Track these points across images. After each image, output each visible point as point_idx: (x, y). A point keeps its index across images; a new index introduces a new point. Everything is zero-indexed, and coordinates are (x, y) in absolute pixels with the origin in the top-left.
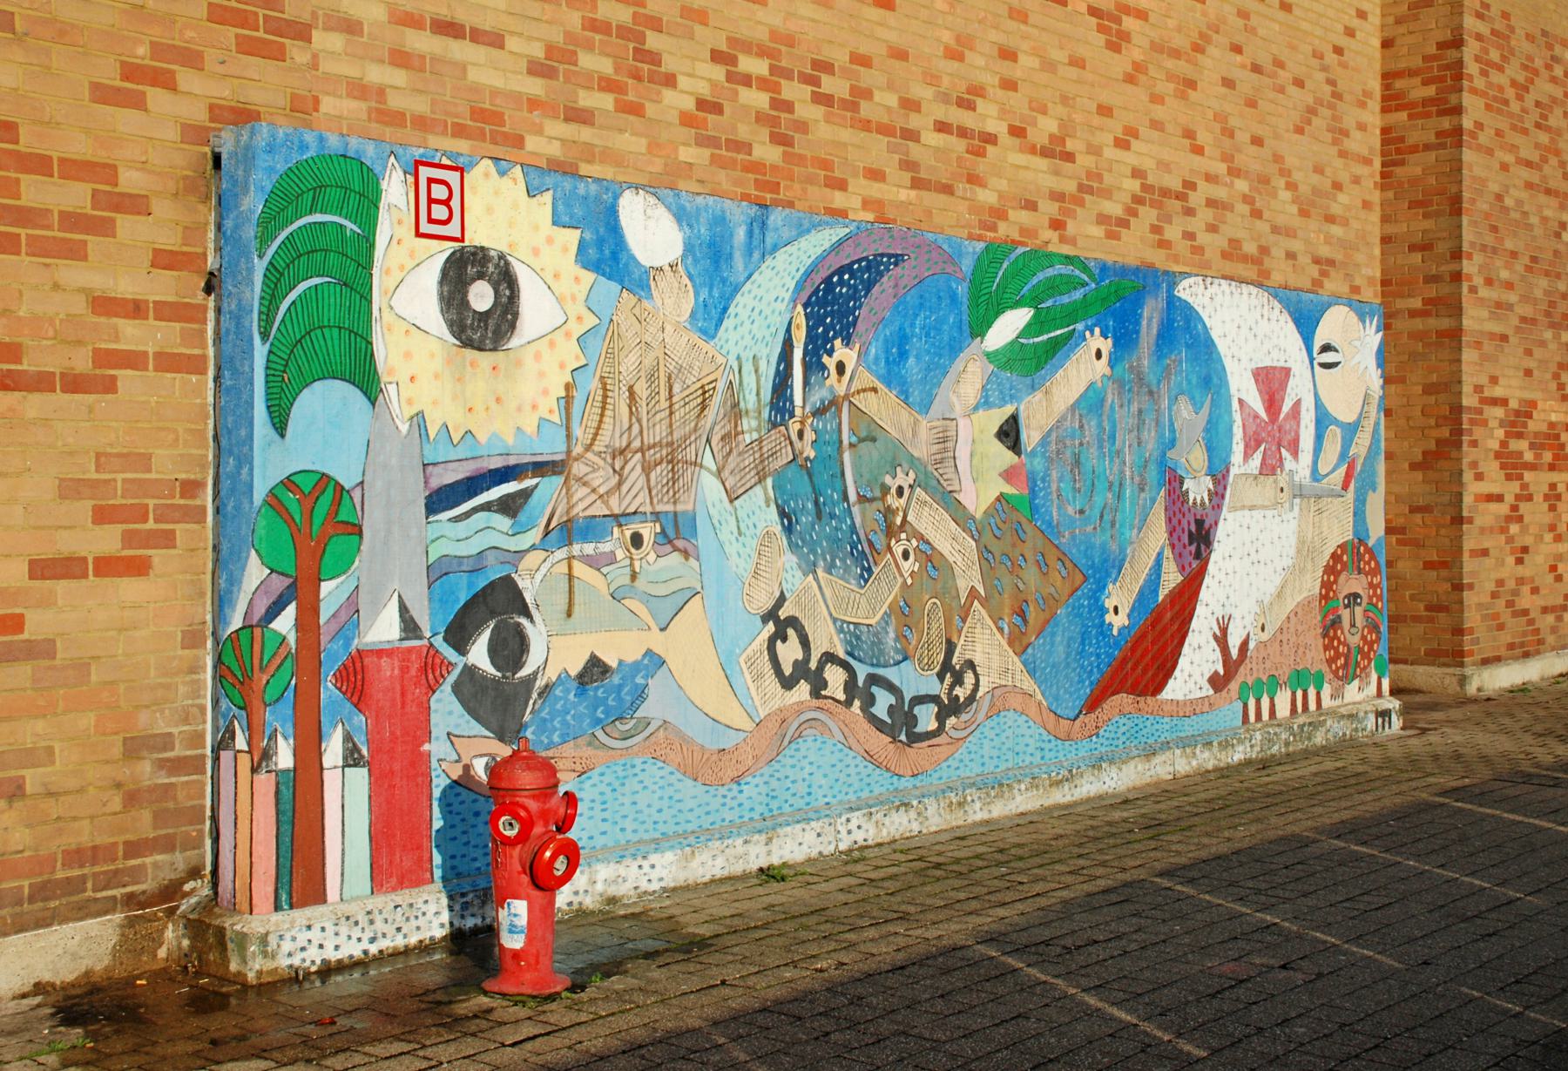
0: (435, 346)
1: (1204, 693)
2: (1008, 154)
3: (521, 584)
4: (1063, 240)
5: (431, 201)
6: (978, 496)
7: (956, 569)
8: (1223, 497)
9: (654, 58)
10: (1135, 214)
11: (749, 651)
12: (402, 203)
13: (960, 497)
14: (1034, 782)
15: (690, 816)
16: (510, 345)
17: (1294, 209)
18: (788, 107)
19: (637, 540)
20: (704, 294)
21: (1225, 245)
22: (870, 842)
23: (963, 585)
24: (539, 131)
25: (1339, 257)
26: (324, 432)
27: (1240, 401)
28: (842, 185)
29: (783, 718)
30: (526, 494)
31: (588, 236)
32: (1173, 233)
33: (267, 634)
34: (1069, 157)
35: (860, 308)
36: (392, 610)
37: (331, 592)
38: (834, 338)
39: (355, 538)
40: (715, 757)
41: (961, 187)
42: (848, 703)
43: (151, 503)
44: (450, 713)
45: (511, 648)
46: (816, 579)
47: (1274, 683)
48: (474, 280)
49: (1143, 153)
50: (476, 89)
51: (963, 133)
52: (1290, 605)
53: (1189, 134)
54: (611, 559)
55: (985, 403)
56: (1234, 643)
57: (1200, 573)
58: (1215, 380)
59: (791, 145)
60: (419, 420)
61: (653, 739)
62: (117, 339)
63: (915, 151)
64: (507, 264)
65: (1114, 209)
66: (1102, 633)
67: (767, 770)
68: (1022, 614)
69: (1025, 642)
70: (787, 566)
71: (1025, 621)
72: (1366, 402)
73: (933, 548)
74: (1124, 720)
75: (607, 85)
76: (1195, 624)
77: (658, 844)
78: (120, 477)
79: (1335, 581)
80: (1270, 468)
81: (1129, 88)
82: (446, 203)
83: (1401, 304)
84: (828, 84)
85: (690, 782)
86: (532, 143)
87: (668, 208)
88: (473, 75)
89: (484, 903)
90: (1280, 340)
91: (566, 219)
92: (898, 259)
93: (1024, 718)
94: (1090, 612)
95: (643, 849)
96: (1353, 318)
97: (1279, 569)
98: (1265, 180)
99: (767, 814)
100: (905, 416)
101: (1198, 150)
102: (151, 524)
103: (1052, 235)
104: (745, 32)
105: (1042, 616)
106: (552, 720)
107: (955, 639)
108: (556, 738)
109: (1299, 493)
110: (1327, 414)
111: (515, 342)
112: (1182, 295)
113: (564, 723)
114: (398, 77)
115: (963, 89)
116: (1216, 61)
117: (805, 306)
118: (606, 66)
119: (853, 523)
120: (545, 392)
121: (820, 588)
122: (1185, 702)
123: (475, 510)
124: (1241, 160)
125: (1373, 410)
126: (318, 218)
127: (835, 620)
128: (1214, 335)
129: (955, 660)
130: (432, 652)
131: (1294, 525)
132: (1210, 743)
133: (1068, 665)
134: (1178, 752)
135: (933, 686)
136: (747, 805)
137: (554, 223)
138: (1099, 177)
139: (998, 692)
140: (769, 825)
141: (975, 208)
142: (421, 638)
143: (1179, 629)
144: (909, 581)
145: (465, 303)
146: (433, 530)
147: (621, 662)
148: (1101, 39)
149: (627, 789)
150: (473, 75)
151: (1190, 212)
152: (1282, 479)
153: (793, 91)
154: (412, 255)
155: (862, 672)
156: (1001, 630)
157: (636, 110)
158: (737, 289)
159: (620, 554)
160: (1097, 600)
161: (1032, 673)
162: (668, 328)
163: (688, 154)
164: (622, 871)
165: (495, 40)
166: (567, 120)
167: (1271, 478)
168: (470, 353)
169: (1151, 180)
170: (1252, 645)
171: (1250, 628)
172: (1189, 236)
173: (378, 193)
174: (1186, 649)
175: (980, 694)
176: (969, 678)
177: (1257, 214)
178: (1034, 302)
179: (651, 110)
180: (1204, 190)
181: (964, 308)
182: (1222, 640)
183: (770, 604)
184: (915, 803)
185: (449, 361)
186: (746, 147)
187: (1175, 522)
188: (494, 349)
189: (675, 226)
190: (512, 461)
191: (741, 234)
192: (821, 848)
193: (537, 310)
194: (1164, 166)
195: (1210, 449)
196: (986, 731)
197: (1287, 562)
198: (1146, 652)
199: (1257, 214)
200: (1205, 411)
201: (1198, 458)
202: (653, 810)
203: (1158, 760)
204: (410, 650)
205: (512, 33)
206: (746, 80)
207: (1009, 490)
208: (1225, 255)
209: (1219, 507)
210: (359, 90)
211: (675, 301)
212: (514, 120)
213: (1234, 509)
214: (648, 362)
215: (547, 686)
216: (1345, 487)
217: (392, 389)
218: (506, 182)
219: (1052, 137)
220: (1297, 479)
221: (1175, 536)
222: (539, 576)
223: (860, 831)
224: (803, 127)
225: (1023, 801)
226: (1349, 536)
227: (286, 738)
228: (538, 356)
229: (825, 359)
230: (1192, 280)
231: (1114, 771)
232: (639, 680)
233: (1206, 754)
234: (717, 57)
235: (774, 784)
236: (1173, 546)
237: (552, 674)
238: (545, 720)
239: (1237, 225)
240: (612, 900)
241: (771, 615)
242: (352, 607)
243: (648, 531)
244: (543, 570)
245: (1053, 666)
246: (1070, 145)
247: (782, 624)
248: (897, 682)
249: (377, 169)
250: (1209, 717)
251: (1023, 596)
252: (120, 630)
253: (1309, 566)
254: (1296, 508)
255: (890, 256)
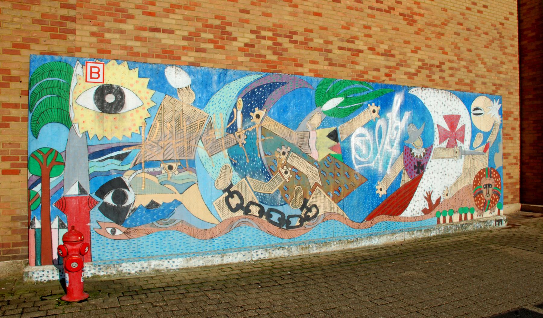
0: (92, 113)
1: (420, 215)
2: (371, 56)
3: (124, 179)
4: (390, 80)
5: (91, 73)
6: (319, 155)
7: (309, 177)
8: (430, 155)
9: (229, 33)
10: (420, 72)
11: (218, 200)
12: (81, 73)
13: (311, 155)
14: (340, 242)
15: (192, 248)
16: (121, 112)
17: (485, 70)
18: (280, 44)
19: (170, 168)
20: (199, 95)
21: (457, 80)
22: (266, 258)
23: (312, 182)
24: (186, 55)
25: (503, 83)
26: (51, 136)
27: (438, 125)
28: (301, 66)
29: (232, 221)
30: (127, 154)
31: (152, 80)
32: (435, 77)
33: (31, 192)
34: (393, 56)
35: (266, 98)
36: (76, 186)
37: (54, 181)
38: (255, 107)
39: (63, 166)
40: (203, 231)
41: (348, 65)
42: (261, 216)
43: (20, 156)
44: (98, 215)
45: (120, 197)
46: (246, 180)
47: (452, 212)
48: (107, 94)
49: (421, 54)
50: (164, 45)
51: (349, 50)
52: (459, 188)
53: (441, 49)
54: (160, 173)
55: (323, 126)
56: (434, 199)
57: (420, 177)
58: (427, 119)
59: (281, 55)
60: (86, 134)
61: (177, 225)
62: (10, 114)
63: (330, 55)
64: (120, 89)
65: (412, 70)
66: (374, 196)
67: (225, 236)
68: (339, 191)
69: (339, 199)
70: (234, 176)
71: (340, 193)
72: (494, 124)
73: (298, 170)
74: (384, 223)
75: (210, 41)
76: (416, 193)
77: (177, 256)
78: (10, 149)
79: (480, 180)
80: (450, 146)
81: (416, 36)
82: (98, 73)
83: (526, 97)
84: (295, 38)
85: (192, 239)
86: (183, 58)
87: (186, 71)
88: (163, 41)
89: (107, 269)
90: (456, 106)
91: (143, 75)
92: (283, 84)
93: (338, 222)
94: (369, 190)
95: (171, 256)
96: (488, 100)
97: (455, 177)
98: (472, 61)
99: (225, 248)
100: (286, 131)
101: (446, 53)
102: (20, 161)
103: (387, 78)
104: (263, 24)
105: (347, 192)
106: (136, 218)
107: (308, 198)
108: (138, 224)
109: (464, 153)
110: (477, 129)
111: (123, 111)
112: (412, 93)
113: (141, 219)
114: (138, 44)
115: (350, 37)
116: (452, 27)
117: (243, 98)
118: (211, 36)
119: (263, 163)
120: (134, 125)
121: (248, 182)
122: (411, 218)
123: (107, 159)
124: (462, 56)
125: (497, 128)
126: (50, 79)
127: (254, 192)
128: (426, 105)
129: (308, 204)
130: (91, 198)
131: (462, 163)
132: (421, 230)
133: (358, 206)
134: (406, 233)
135: (298, 212)
136: (217, 245)
137: (139, 77)
138: (405, 62)
139: (326, 214)
140: (223, 253)
141: (354, 71)
142: (87, 194)
143: (409, 195)
144: (288, 180)
145: (104, 101)
146: (90, 164)
147: (164, 203)
148: (405, 22)
149: (166, 239)
150: (163, 41)
151: (442, 71)
152: (456, 149)
153: (285, 42)
154: (84, 88)
155: (266, 208)
156: (329, 196)
157: (223, 48)
158: (213, 94)
159: (163, 172)
160: (372, 187)
161: (343, 209)
162: (184, 106)
163: (241, 59)
164: (161, 262)
165: (172, 32)
166: (196, 51)
167: (452, 149)
168: (105, 115)
169: (426, 62)
170: (442, 200)
171: (441, 195)
172: (443, 78)
173: (73, 71)
174: (412, 201)
175: (319, 214)
176: (314, 210)
177: (470, 71)
178: (345, 95)
179: (227, 47)
180: (448, 64)
181: (313, 97)
182: (428, 198)
183: (226, 187)
184: (287, 247)
185: (98, 117)
186: (264, 56)
187: (407, 162)
188: (115, 113)
189: (188, 76)
190: (121, 145)
191: (215, 78)
192: (245, 259)
193: (131, 101)
194: (432, 58)
195: (424, 140)
196: (322, 226)
197: (458, 175)
198: (393, 203)
199: (470, 71)
200: (422, 128)
201: (419, 142)
202: (177, 246)
203: (397, 235)
204: (82, 197)
205: (177, 30)
206: (264, 38)
207: (332, 152)
208: (456, 83)
209: (428, 158)
210: (124, 48)
211: (187, 99)
212: (177, 52)
213: (433, 159)
214: (176, 115)
215: (134, 209)
216: (485, 151)
217: (76, 125)
218: (121, 66)
219: (385, 50)
220: (463, 149)
221: (408, 167)
222: (131, 178)
223: (261, 255)
224: (286, 50)
225: (334, 247)
226: (486, 166)
227: (38, 220)
228: (132, 115)
229: (251, 114)
230: (416, 89)
231: (377, 239)
232: (171, 208)
233: (419, 233)
234: (252, 32)
235: (228, 239)
236: (407, 170)
237: (136, 205)
238: (133, 219)
239: (462, 74)
240: (158, 271)
241: (227, 190)
242: (61, 186)
243: (175, 165)
244: (133, 176)
245: (352, 206)
246: (393, 52)
247: (230, 192)
248: (282, 211)
249: (72, 65)
250: (422, 222)
251: (339, 185)
252: (10, 189)
253: (468, 175)
254: (463, 159)
255: (280, 83)
